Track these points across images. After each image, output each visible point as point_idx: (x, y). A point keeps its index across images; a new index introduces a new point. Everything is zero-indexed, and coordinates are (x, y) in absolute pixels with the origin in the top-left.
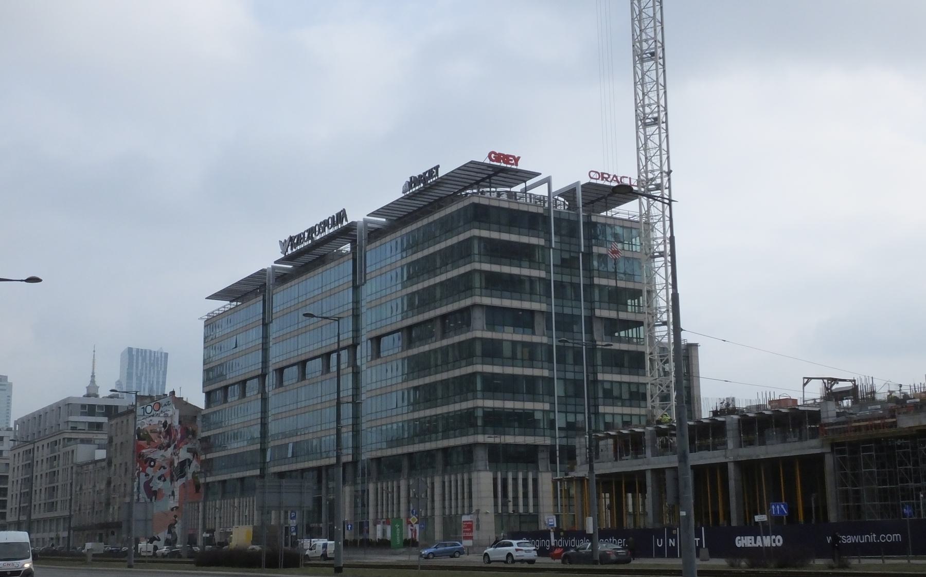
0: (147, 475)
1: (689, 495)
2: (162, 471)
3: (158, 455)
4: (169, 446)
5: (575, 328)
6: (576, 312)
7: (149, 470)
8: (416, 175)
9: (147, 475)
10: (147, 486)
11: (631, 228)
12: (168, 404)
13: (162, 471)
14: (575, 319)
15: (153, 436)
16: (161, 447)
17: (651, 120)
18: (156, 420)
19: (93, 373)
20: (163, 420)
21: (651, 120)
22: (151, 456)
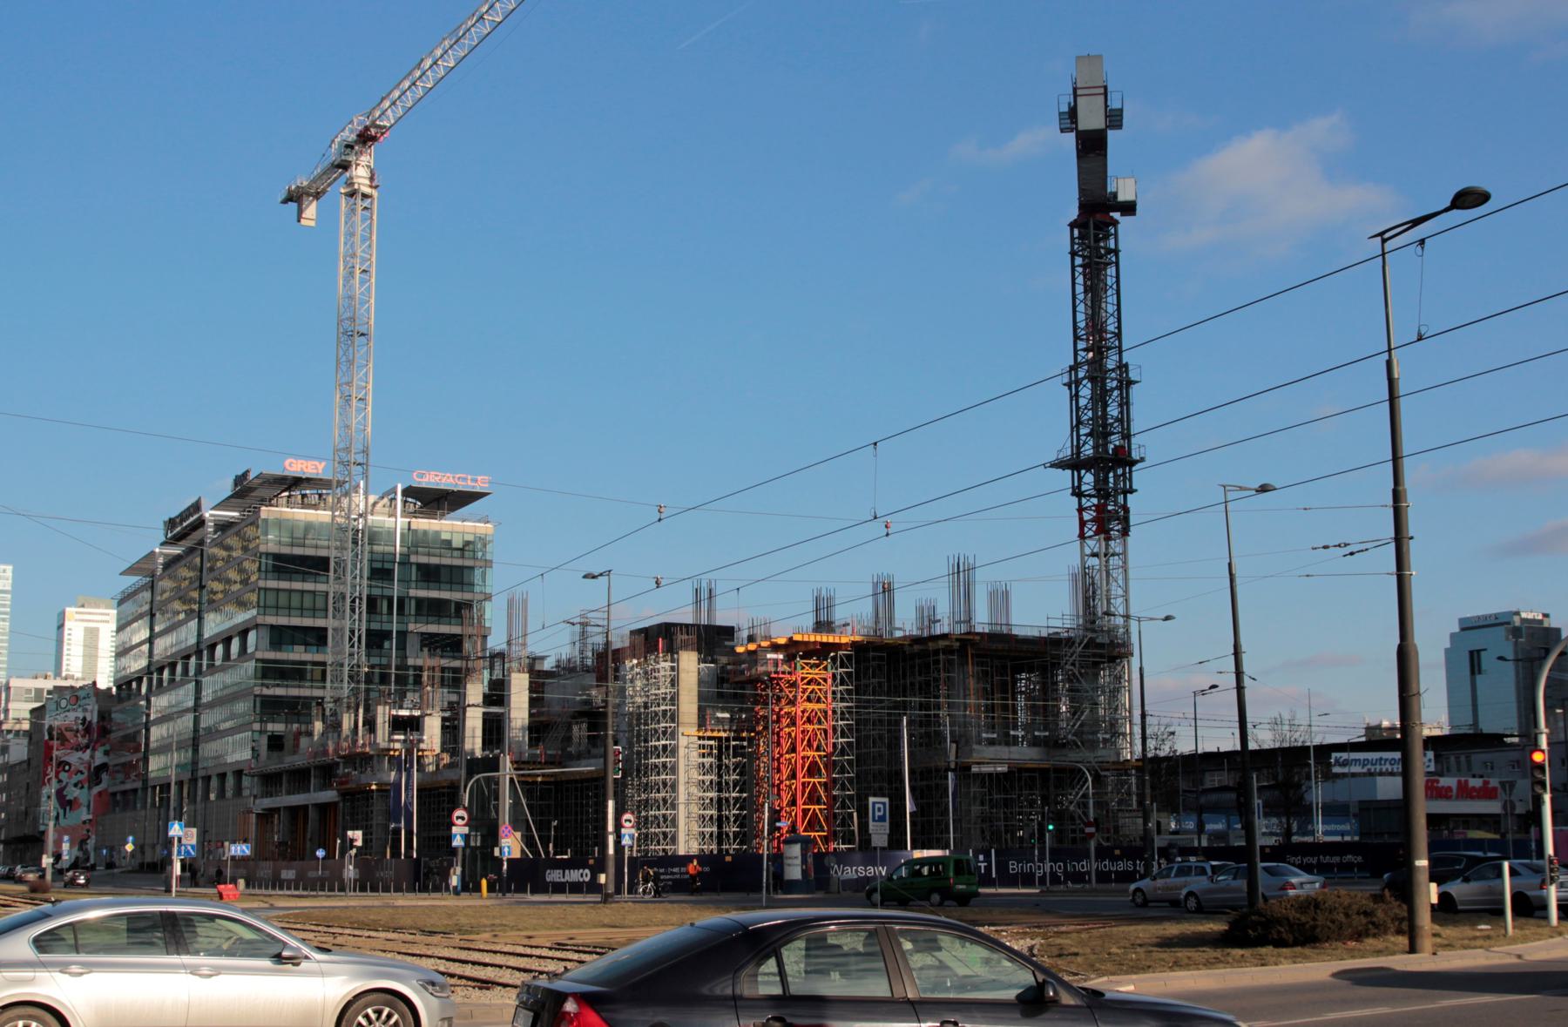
0: (60, 781)
1: (308, 622)
2: (80, 777)
3: (74, 758)
4: (87, 747)
5: (387, 645)
6: (386, 627)
7: (63, 776)
8: (1073, 213)
9: (60, 781)
10: (60, 794)
11: (292, 545)
12: (88, 696)
13: (80, 777)
14: (387, 635)
15: (68, 735)
16: (78, 748)
17: (1103, 467)
18: (72, 715)
19: (1095, 289)
20: (81, 715)
21: (1103, 467)
22: (65, 759)
